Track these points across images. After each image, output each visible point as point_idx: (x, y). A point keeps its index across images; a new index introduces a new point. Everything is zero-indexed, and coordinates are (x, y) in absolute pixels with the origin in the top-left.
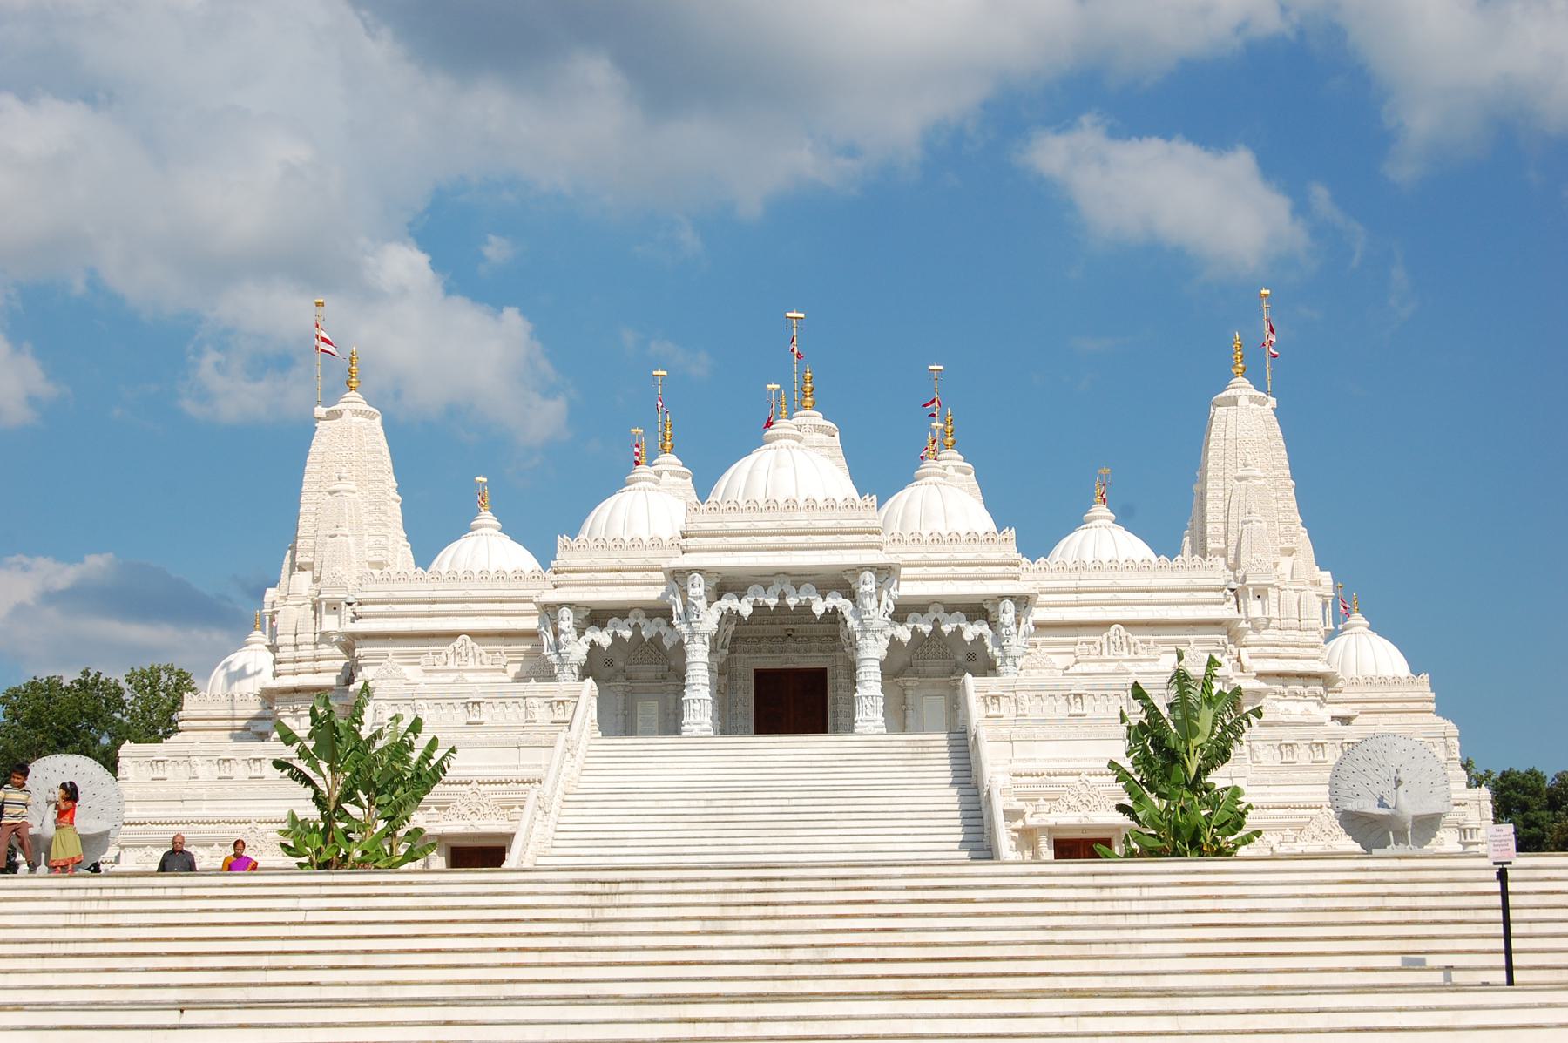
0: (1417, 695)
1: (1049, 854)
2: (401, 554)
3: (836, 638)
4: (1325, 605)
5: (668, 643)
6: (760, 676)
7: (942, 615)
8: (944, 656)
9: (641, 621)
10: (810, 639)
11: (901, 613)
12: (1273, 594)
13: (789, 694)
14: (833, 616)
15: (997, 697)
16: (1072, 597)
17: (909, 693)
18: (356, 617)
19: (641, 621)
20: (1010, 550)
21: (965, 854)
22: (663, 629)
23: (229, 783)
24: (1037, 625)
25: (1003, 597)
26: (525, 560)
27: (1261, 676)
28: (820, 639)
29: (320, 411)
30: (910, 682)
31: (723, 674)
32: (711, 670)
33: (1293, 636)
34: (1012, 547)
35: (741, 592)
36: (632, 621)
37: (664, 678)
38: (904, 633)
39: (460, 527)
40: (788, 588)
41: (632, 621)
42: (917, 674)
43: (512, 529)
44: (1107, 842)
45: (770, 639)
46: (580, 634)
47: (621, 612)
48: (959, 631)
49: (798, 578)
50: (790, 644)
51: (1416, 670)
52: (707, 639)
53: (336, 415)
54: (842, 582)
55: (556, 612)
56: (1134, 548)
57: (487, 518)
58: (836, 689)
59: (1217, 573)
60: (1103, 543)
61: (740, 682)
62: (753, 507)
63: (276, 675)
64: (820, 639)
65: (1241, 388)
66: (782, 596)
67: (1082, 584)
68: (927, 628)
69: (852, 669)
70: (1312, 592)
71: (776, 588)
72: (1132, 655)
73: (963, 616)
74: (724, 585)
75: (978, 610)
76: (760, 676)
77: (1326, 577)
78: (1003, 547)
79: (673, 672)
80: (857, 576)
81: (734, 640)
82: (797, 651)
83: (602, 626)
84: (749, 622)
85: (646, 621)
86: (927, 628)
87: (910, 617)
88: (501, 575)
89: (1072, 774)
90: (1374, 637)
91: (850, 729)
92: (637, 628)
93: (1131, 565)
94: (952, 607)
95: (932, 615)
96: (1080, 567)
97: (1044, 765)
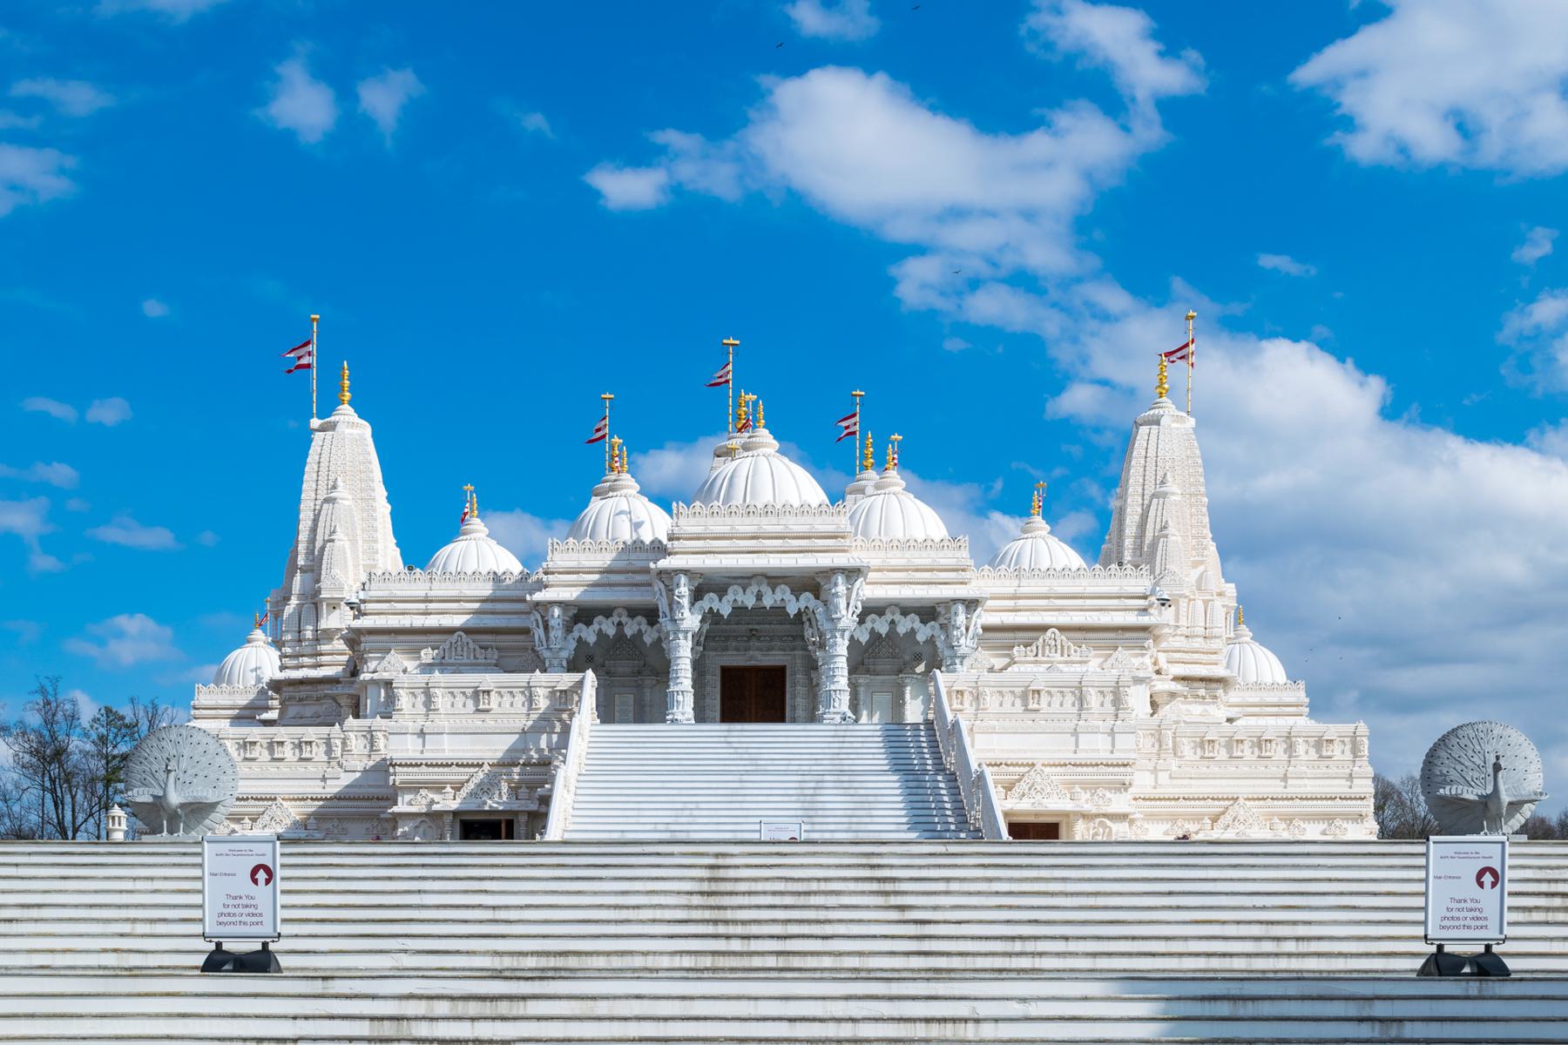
0: (1292, 700)
1: (1005, 835)
2: (389, 556)
6: (726, 671)
7: (897, 617)
9: (624, 619)
10: (727, 638)
11: (871, 610)
12: (1183, 603)
13: (754, 691)
15: (1038, 692)
16: (1011, 603)
17: (862, 689)
18: (360, 614)
19: (624, 619)
20: (963, 556)
21: (913, 836)
23: (309, 764)
24: (986, 629)
25: (955, 601)
27: (1175, 679)
28: (781, 638)
29: (315, 423)
31: (698, 666)
33: (1198, 643)
34: (965, 553)
35: (721, 591)
36: (616, 619)
37: (639, 673)
39: (453, 528)
40: (765, 589)
41: (616, 619)
42: (868, 672)
44: (510, 824)
46: (568, 629)
48: (913, 632)
49: (773, 579)
50: (755, 643)
51: (1293, 678)
52: (690, 635)
53: (332, 427)
54: (813, 584)
55: (547, 610)
58: (794, 685)
59: (1138, 583)
60: (1044, 550)
63: (282, 668)
65: (346, 414)
66: (759, 597)
67: (1022, 590)
68: (611, 631)
69: (812, 666)
71: (754, 589)
72: (1065, 658)
73: (917, 618)
74: (705, 585)
75: (928, 612)
76: (726, 671)
78: (958, 554)
79: (662, 671)
83: (588, 623)
84: (728, 622)
85: (629, 621)
86: (611, 631)
87: (596, 620)
89: (473, 765)
90: (1257, 647)
91: (812, 718)
93: (1065, 572)
94: (906, 609)
95: (889, 617)
97: (1005, 756)
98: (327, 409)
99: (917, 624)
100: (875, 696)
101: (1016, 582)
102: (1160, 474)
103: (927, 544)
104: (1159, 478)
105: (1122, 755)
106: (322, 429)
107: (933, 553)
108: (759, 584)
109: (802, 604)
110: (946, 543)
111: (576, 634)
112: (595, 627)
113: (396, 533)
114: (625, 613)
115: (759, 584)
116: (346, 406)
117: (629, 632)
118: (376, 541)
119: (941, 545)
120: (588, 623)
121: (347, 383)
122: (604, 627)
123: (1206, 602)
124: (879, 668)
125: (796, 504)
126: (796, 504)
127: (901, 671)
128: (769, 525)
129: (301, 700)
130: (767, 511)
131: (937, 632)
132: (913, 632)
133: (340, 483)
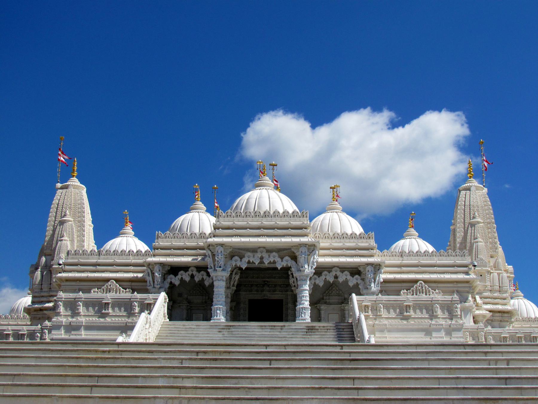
3: (288, 285)
4: (510, 281)
5: (207, 283)
7: (338, 273)
8: (339, 295)
9: (195, 273)
10: (252, 285)
14: (286, 270)
17: (322, 312)
22: (205, 277)
26: (143, 247)
28: (280, 286)
29: (59, 185)
30: (323, 307)
32: (227, 297)
38: (320, 282)
42: (326, 303)
43: (139, 235)
45: (257, 285)
47: (185, 268)
53: (66, 187)
54: (291, 252)
56: (426, 247)
57: (129, 229)
61: (242, 305)
62: (247, 215)
64: (280, 286)
65: (75, 182)
68: (187, 279)
69: (295, 300)
70: (505, 275)
75: (355, 271)
77: (510, 268)
80: (298, 249)
81: (238, 286)
82: (269, 291)
83: (176, 275)
85: (197, 274)
86: (187, 279)
88: (130, 253)
92: (192, 276)
93: (426, 254)
94: (343, 268)
95: (333, 273)
96: (402, 254)
98: (65, 178)
99: (349, 277)
100: (330, 316)
101: (401, 259)
102: (472, 213)
103: (353, 236)
104: (472, 216)
105: (456, 339)
106: (62, 188)
107: (356, 241)
108: (262, 252)
109: (284, 264)
110: (362, 236)
111: (169, 280)
112: (179, 276)
113: (95, 239)
114: (195, 269)
115: (262, 252)
116: (75, 178)
117: (197, 279)
118: (83, 241)
119: (361, 237)
120: (176, 275)
121: (76, 168)
122: (184, 277)
123: (499, 274)
124: (331, 301)
125: (281, 211)
126: (281, 211)
127: (343, 303)
128: (266, 222)
129: (39, 319)
130: (266, 214)
131: (359, 281)
132: (346, 282)
133: (68, 212)
